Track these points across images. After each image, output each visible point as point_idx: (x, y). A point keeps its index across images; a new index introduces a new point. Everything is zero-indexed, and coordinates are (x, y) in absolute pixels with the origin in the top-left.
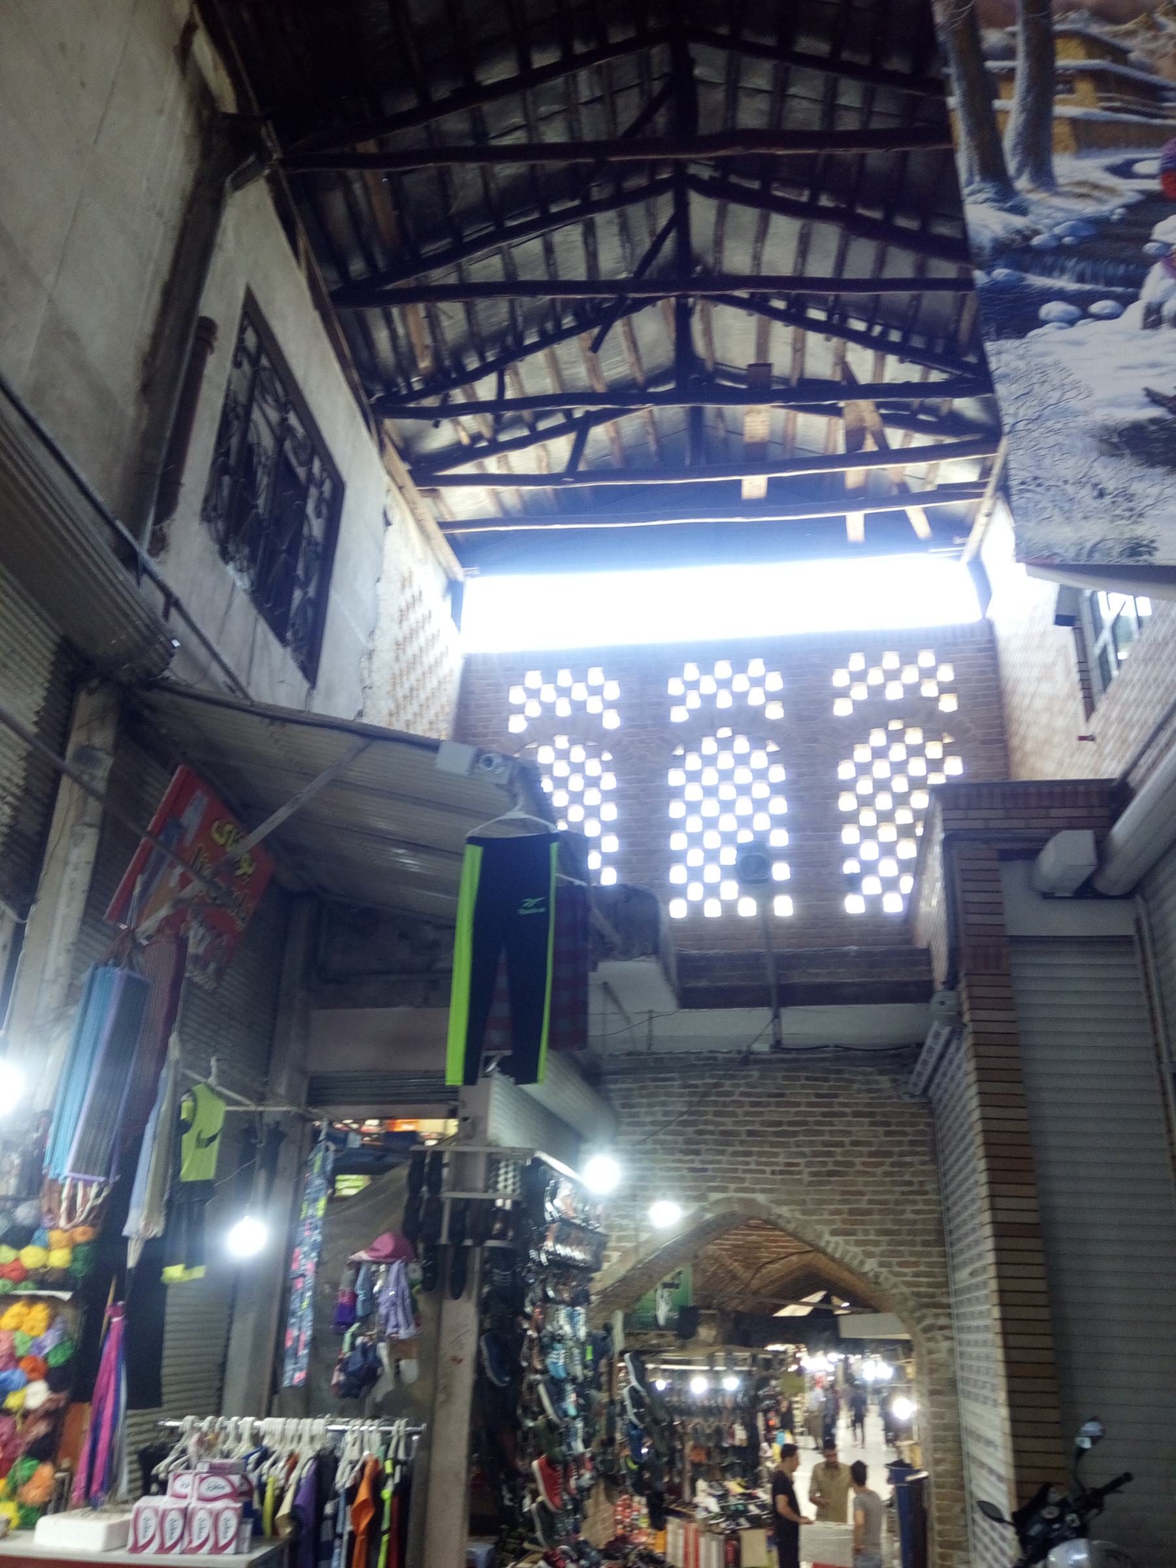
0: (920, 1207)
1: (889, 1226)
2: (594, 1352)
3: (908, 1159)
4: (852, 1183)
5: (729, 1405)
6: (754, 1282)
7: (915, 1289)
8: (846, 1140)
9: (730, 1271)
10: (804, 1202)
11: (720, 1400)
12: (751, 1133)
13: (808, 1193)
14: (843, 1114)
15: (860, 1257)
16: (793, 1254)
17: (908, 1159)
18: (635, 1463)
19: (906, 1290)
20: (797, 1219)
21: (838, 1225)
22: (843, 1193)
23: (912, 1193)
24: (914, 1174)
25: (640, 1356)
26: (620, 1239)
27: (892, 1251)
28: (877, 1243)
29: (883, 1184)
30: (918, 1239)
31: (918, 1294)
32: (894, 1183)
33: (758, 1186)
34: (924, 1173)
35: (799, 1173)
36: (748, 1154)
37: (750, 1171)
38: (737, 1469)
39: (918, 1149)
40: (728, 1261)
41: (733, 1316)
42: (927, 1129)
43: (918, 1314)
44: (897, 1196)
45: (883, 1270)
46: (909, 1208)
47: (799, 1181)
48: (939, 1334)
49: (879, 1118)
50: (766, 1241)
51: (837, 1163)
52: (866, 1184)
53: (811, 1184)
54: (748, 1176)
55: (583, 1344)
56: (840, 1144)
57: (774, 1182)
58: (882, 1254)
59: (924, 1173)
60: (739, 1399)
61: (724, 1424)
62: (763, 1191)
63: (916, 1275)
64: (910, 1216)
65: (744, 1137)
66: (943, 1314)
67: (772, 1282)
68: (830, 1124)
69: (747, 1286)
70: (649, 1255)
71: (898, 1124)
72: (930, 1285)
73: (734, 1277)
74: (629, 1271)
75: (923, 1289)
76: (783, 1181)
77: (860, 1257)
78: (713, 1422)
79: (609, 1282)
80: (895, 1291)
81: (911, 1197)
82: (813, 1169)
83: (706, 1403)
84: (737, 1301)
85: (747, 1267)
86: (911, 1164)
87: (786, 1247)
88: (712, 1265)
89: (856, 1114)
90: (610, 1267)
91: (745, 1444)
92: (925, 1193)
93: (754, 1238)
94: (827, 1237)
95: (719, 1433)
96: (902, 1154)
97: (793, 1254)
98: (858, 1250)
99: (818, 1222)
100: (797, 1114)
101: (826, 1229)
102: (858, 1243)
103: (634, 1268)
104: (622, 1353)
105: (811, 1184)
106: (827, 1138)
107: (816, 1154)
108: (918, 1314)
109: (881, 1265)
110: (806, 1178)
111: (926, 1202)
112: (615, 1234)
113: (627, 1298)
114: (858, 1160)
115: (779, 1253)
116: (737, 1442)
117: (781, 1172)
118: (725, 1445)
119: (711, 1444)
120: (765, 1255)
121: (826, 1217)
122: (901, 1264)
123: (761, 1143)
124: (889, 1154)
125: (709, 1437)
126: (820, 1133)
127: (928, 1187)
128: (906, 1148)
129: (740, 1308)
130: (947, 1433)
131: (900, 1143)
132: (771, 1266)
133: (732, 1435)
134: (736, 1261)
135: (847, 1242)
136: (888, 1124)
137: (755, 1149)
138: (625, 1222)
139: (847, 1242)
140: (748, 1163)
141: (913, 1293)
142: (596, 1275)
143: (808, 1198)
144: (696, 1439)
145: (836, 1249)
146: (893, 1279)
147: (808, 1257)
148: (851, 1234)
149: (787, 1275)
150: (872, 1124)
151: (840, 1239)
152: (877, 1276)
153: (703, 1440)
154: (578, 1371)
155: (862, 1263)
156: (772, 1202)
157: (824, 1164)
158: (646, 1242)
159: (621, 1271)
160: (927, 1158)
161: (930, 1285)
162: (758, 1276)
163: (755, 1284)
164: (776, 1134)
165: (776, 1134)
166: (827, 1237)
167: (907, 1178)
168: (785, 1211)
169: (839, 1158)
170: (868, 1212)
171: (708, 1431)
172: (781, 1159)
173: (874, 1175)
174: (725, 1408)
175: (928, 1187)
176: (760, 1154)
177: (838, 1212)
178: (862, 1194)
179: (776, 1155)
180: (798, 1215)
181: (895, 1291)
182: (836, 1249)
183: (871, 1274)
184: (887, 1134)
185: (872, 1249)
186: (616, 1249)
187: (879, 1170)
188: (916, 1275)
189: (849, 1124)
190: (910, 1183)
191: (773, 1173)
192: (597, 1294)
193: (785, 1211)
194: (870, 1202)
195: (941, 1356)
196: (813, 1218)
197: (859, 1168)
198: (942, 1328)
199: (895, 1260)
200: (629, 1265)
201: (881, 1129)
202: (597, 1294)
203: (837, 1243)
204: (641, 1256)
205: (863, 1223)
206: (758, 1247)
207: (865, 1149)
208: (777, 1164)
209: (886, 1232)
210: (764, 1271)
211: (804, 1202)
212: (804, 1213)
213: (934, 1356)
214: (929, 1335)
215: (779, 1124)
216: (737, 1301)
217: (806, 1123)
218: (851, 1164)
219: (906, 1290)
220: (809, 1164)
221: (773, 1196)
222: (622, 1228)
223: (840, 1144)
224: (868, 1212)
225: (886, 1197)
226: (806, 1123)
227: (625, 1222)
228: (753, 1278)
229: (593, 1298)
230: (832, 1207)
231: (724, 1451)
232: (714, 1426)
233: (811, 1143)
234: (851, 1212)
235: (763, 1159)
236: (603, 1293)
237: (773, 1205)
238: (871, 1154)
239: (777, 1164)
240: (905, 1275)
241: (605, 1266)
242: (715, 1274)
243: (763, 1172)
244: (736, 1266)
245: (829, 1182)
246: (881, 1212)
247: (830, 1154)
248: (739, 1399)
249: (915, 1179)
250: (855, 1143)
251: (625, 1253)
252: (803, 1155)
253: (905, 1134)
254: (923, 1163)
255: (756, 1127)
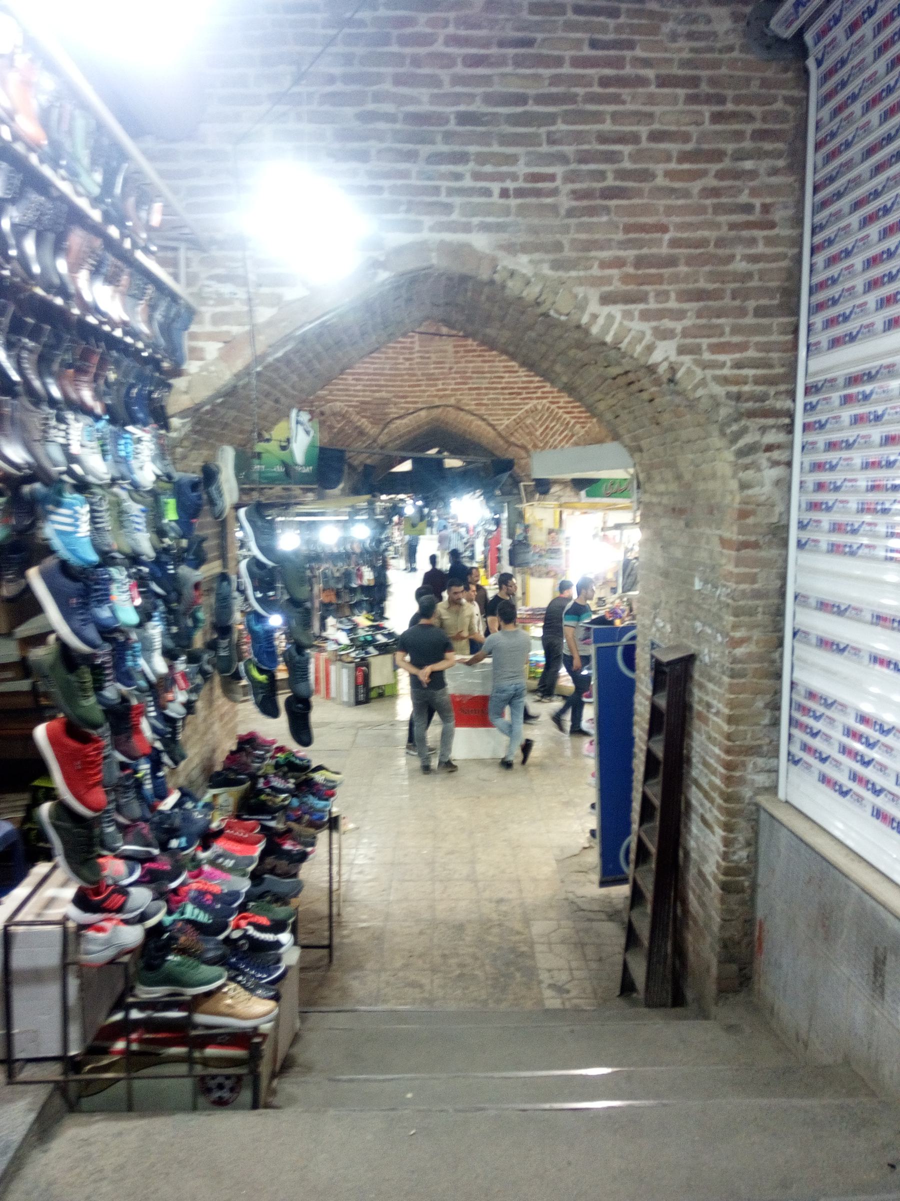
0: (760, 249)
1: (702, 284)
2: (180, 508)
3: (748, 165)
4: (646, 210)
5: (358, 550)
6: (381, 437)
7: (734, 389)
8: (643, 130)
9: (357, 428)
10: (558, 247)
11: (348, 547)
12: (465, 119)
13: (566, 229)
14: (641, 81)
15: (648, 338)
16: (422, 409)
17: (748, 165)
18: (261, 671)
19: (719, 391)
20: (544, 278)
21: (617, 286)
22: (628, 229)
23: (749, 225)
24: (754, 192)
25: (259, 511)
26: (218, 319)
27: (703, 326)
28: (679, 315)
29: (702, 210)
30: (751, 304)
31: (738, 397)
32: (718, 209)
33: (476, 220)
34: (773, 190)
35: (554, 192)
36: (461, 158)
37: (461, 192)
38: (364, 605)
39: (768, 146)
40: (355, 418)
41: (360, 469)
42: (789, 108)
43: (735, 427)
44: (724, 231)
45: (687, 359)
46: (739, 251)
47: (554, 208)
48: (762, 458)
49: (705, 88)
50: (394, 397)
51: (622, 174)
52: (670, 211)
53: (571, 213)
54: (457, 200)
55: (154, 494)
56: (634, 138)
57: (507, 211)
58: (685, 333)
59: (773, 190)
60: (367, 545)
61: (352, 567)
62: (485, 228)
63: (738, 365)
64: (740, 266)
65: (452, 126)
66: (773, 427)
67: (400, 437)
68: (616, 99)
69: (375, 441)
70: (274, 347)
71: (737, 100)
72: (757, 381)
73: (362, 433)
74: (238, 376)
75: (746, 388)
76: (522, 210)
77: (648, 338)
78: (342, 566)
79: (202, 394)
80: (700, 392)
81: (745, 233)
82: (577, 186)
83: (335, 550)
84: (365, 455)
85: (374, 423)
86: (752, 174)
87: (415, 403)
88: (338, 422)
89: (663, 81)
90: (202, 369)
91: (372, 584)
92: (772, 225)
93: (384, 394)
94: (594, 306)
95: (347, 575)
96: (739, 156)
97: (422, 409)
98: (646, 327)
99: (580, 281)
100: (556, 80)
101: (594, 295)
102: (645, 316)
103: (247, 371)
104: (237, 507)
105: (571, 213)
106: (607, 126)
107: (584, 158)
108: (735, 427)
109: (682, 350)
110: (565, 202)
111: (769, 241)
112: (207, 311)
113: (241, 432)
114: (660, 168)
115: (408, 409)
116: (365, 582)
117: (520, 193)
118: (354, 586)
119: (340, 586)
120: (393, 411)
121: (596, 271)
122: (717, 348)
123: (484, 139)
124: (717, 156)
125: (338, 579)
126: (597, 117)
127: (778, 215)
128: (747, 144)
129: (368, 462)
130: (757, 602)
131: (738, 136)
132: (398, 422)
133: (360, 576)
134: (363, 417)
135: (628, 315)
136: (721, 100)
137: (473, 149)
138: (226, 289)
139: (628, 315)
140: (458, 177)
141: (729, 395)
142: (179, 383)
143: (565, 240)
144: (326, 583)
145: (606, 329)
146: (699, 373)
147: (435, 412)
148: (633, 301)
149: (414, 429)
150: (692, 99)
151: (616, 310)
152: (673, 369)
153: (332, 583)
154: (145, 543)
155: (650, 349)
156: (501, 247)
157: (602, 175)
158: (270, 323)
159: (225, 375)
160: (781, 163)
161: (757, 381)
162: (386, 431)
163: (383, 439)
164: (514, 120)
165: (514, 120)
166: (594, 306)
167: (744, 198)
168: (523, 263)
169: (627, 165)
170: (671, 262)
171: (337, 575)
172: (521, 169)
173: (686, 194)
174: (354, 553)
175: (778, 215)
176: (482, 159)
177: (619, 263)
178: (664, 229)
179: (512, 159)
180: (546, 270)
181: (700, 392)
182: (606, 329)
183: (662, 369)
184: (717, 118)
185: (667, 323)
186: (211, 337)
187: (696, 186)
188: (738, 365)
189: (651, 100)
190: (748, 208)
191: (504, 193)
192: (182, 414)
193: (523, 263)
194: (674, 243)
195: (764, 490)
196: (573, 273)
197: (660, 181)
198: (769, 448)
199: (705, 342)
200: (239, 365)
201: (707, 110)
202: (182, 414)
203: (610, 318)
204: (260, 349)
205: (659, 279)
206: (385, 403)
207: (674, 147)
208: (514, 177)
209: (700, 295)
210: (392, 426)
211: (558, 247)
212: (557, 265)
213: (750, 492)
214: (748, 460)
215: (521, 99)
216: (365, 455)
217: (571, 99)
218: (646, 175)
219: (719, 391)
220: (570, 177)
221: (504, 237)
222: (221, 300)
223: (634, 138)
224: (671, 262)
225: (700, 234)
226: (571, 99)
227: (226, 289)
228: (380, 434)
229: (175, 422)
230: (605, 254)
231: (353, 591)
232: (343, 570)
233: (578, 138)
234: (639, 262)
235: (488, 168)
236: (193, 412)
237: (500, 254)
238: (684, 157)
239: (514, 177)
240: (722, 365)
241: (192, 367)
242: (342, 430)
243: (487, 193)
244: (364, 423)
245: (607, 210)
246: (690, 261)
247: (611, 158)
248: (367, 545)
249: (757, 202)
250: (655, 137)
251: (229, 343)
252: (563, 159)
253: (750, 118)
254: (774, 172)
255: (477, 107)
